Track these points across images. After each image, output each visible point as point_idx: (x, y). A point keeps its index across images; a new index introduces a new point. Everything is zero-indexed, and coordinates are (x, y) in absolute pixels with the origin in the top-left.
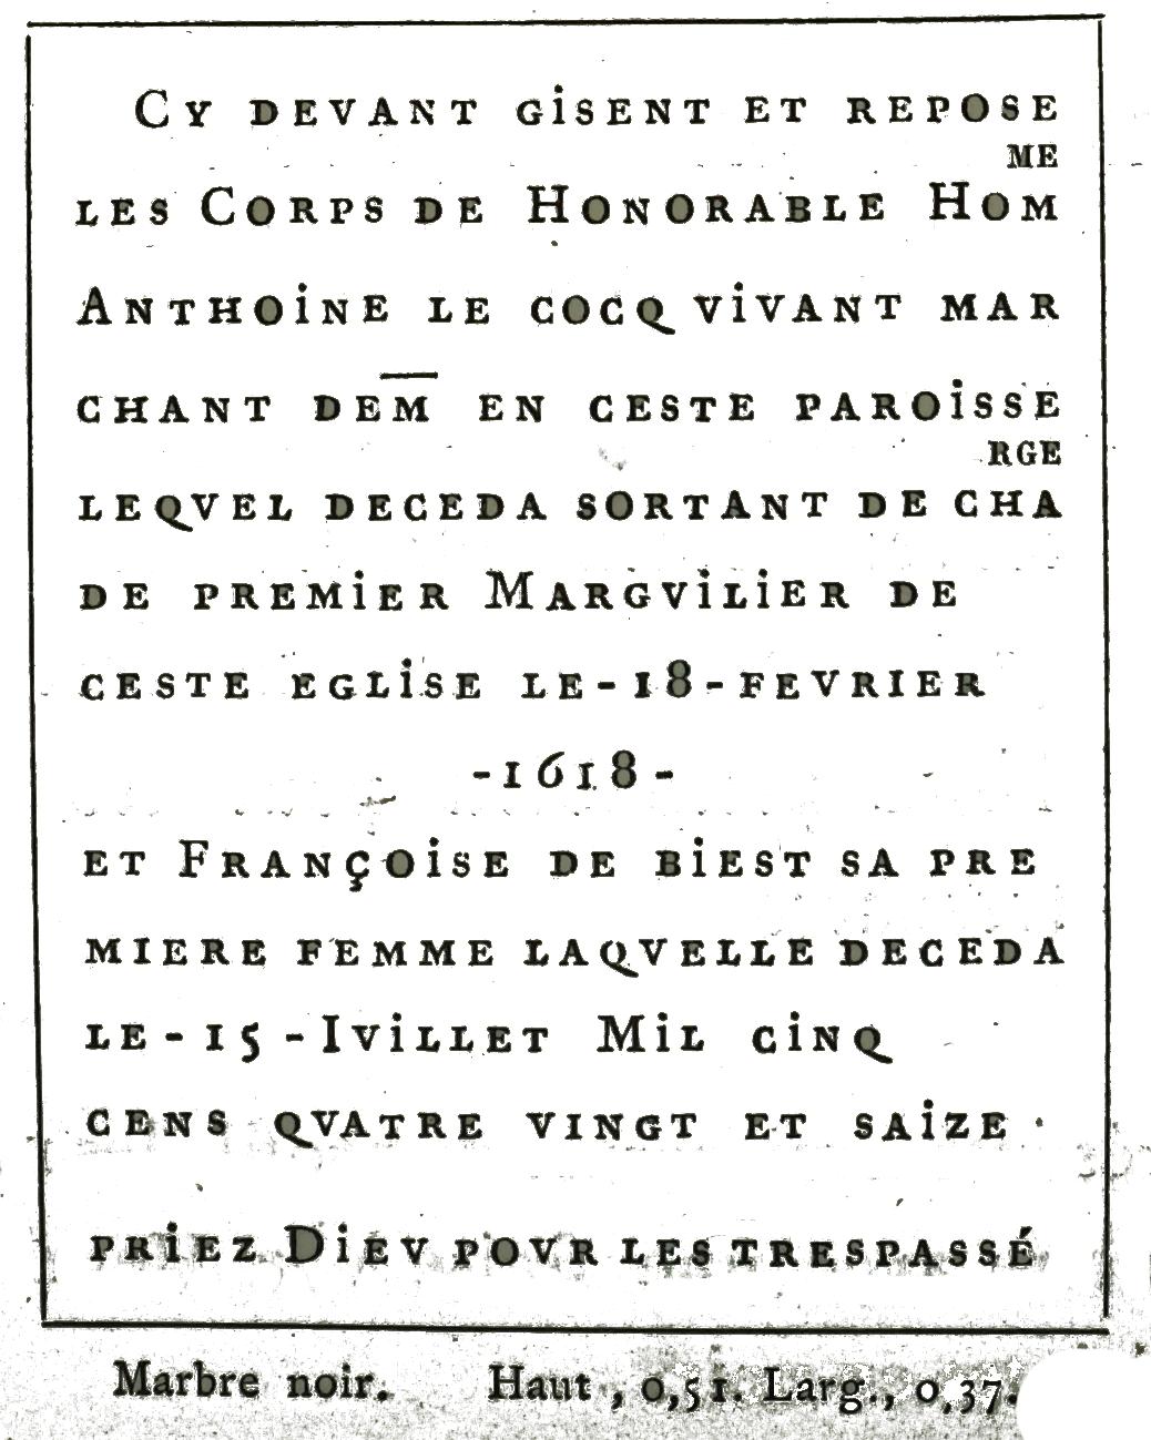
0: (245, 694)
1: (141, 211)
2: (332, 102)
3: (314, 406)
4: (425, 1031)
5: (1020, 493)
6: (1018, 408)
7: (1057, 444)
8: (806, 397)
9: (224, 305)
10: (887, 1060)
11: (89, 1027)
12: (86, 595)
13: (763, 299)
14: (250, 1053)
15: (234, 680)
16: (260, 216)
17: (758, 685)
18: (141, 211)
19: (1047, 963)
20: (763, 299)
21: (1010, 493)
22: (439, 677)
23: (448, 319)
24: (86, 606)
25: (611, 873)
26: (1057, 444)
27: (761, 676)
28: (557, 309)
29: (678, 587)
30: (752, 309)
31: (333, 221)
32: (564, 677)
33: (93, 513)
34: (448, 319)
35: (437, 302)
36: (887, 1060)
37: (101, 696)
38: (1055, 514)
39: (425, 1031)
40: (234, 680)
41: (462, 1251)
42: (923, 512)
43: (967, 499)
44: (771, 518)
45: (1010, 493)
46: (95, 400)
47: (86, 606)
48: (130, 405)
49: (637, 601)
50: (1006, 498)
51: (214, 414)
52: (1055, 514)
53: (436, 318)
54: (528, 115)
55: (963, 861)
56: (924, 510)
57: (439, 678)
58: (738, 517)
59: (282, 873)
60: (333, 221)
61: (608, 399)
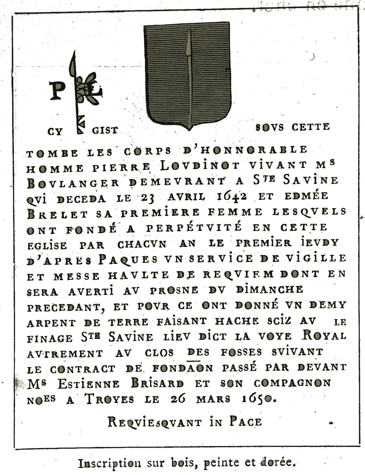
0: (223, 214)
1: (105, 152)
2: (309, 318)
3: (237, 289)
4: (292, 147)
5: (116, 273)
6: (100, 215)
7: (274, 176)
8: (179, 225)
9: (246, 320)
10: (232, 280)
11: (236, 334)
12: (238, 289)
13: (267, 163)
14: (260, 403)
15: (332, 161)
16: (295, 275)
17: (213, 212)
18: (105, 152)
19: (171, 200)
20: (267, 163)
21: (291, 287)
22: (208, 350)
23: (93, 155)
24: (282, 277)
25: (158, 402)
26: (274, 176)
27: (214, 209)
28: (132, 151)
29: (158, 304)
30: (265, 165)
31: (178, 231)
32: (284, 209)
33: (202, 198)
34: (93, 155)
35: (90, 151)
36: (232, 280)
37: (242, 261)
38: (133, 232)
39: (292, 147)
40: (326, 125)
41: (179, 228)
42: (302, 292)
43: (284, 226)
44: (161, 247)
45: (291, 287)
46: (241, 256)
47: (282, 277)
48: (246, 320)
49: (93, 185)
50: (30, 168)
51: (297, 306)
52: (133, 232)
53: (90, 155)
54: (95, 131)
55: (130, 213)
56: (56, 217)
57: (342, 214)
58: (131, 232)
59: (201, 183)
60: (178, 231)
61: (286, 225)
